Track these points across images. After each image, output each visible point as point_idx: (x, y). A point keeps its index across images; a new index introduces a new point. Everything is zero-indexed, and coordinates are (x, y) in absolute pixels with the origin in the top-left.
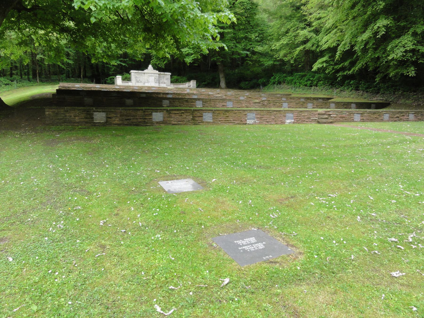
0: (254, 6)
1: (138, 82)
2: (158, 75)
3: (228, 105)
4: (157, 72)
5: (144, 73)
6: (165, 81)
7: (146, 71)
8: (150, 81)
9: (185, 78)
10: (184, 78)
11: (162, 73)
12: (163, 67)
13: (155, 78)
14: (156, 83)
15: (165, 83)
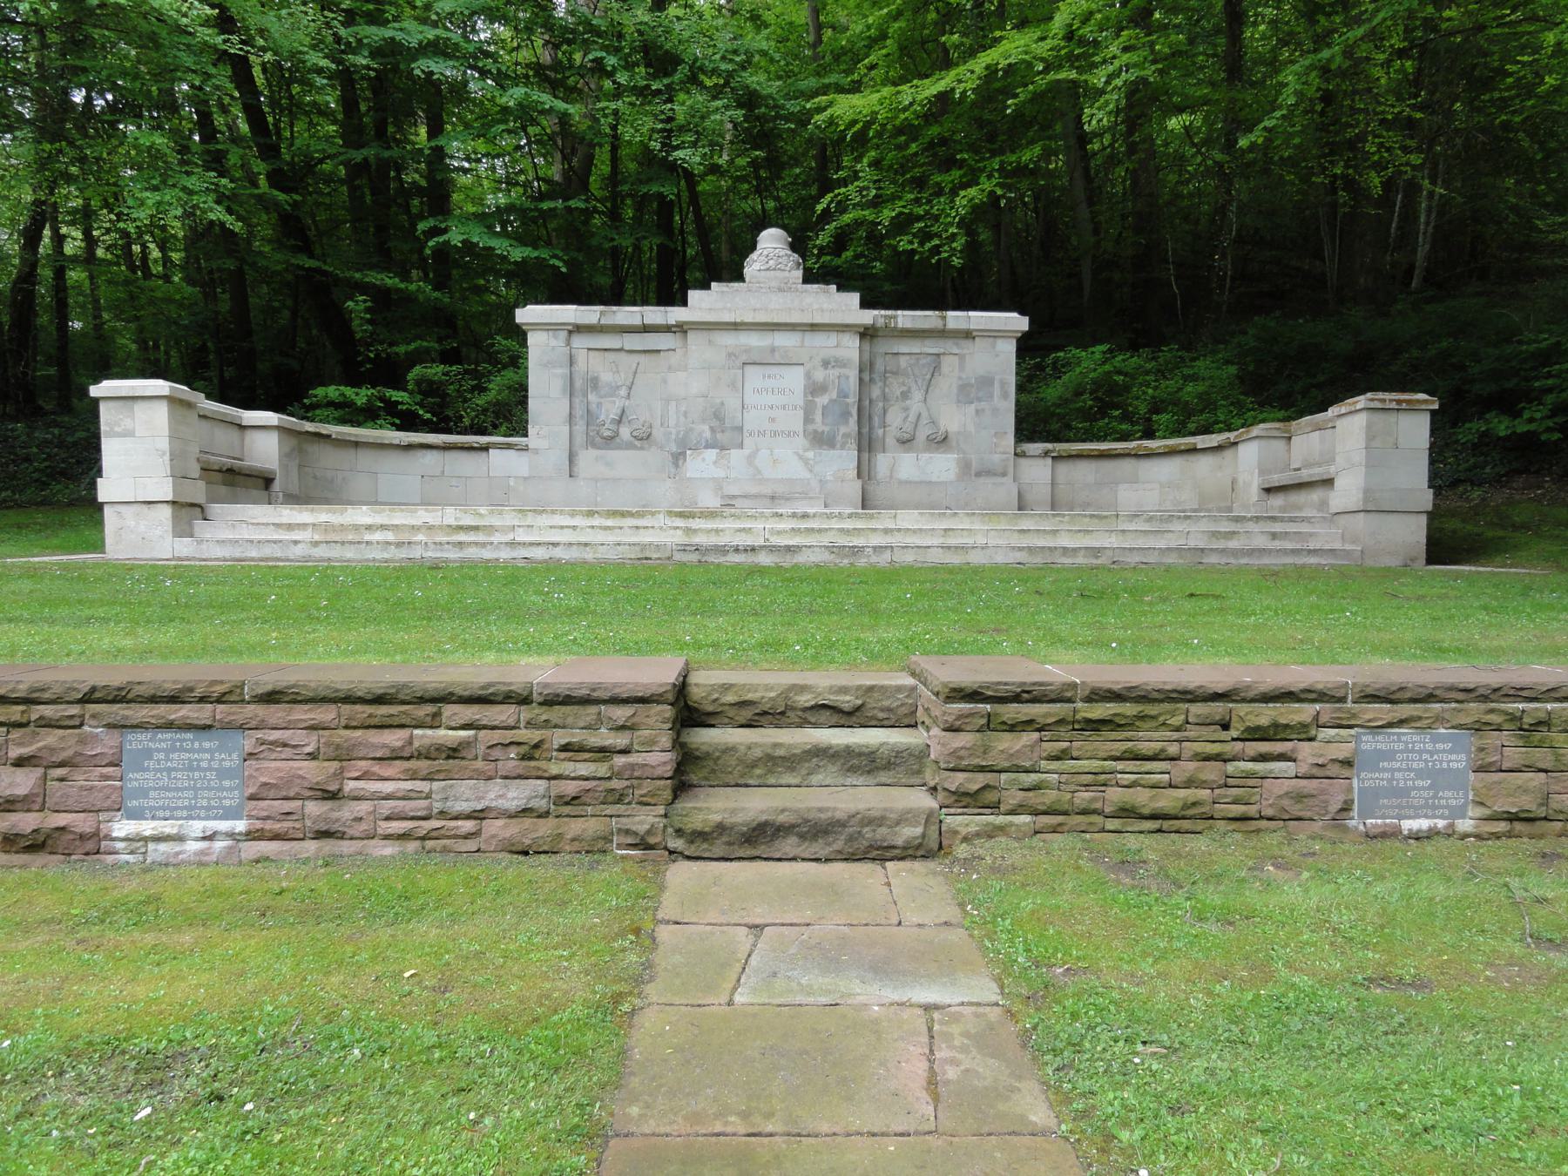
0: (390, 96)
1: (610, 441)
2: (850, 347)
3: (143, 793)
4: (845, 306)
5: (681, 329)
6: (953, 418)
7: (704, 303)
8: (752, 421)
9: (1211, 371)
10: (1202, 366)
11: (905, 318)
12: (954, 253)
13: (814, 389)
14: (821, 441)
15: (941, 442)
